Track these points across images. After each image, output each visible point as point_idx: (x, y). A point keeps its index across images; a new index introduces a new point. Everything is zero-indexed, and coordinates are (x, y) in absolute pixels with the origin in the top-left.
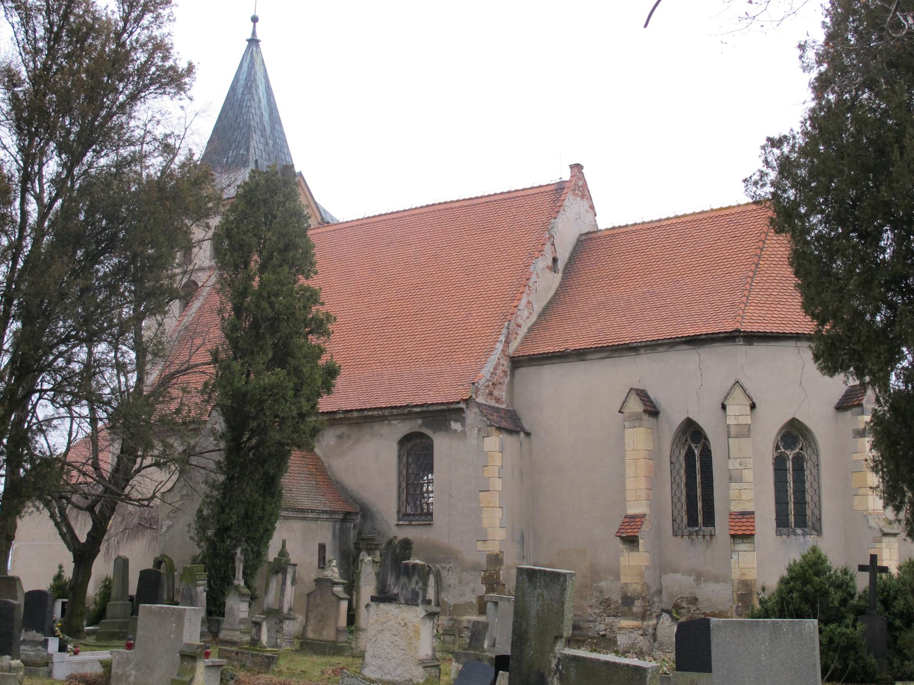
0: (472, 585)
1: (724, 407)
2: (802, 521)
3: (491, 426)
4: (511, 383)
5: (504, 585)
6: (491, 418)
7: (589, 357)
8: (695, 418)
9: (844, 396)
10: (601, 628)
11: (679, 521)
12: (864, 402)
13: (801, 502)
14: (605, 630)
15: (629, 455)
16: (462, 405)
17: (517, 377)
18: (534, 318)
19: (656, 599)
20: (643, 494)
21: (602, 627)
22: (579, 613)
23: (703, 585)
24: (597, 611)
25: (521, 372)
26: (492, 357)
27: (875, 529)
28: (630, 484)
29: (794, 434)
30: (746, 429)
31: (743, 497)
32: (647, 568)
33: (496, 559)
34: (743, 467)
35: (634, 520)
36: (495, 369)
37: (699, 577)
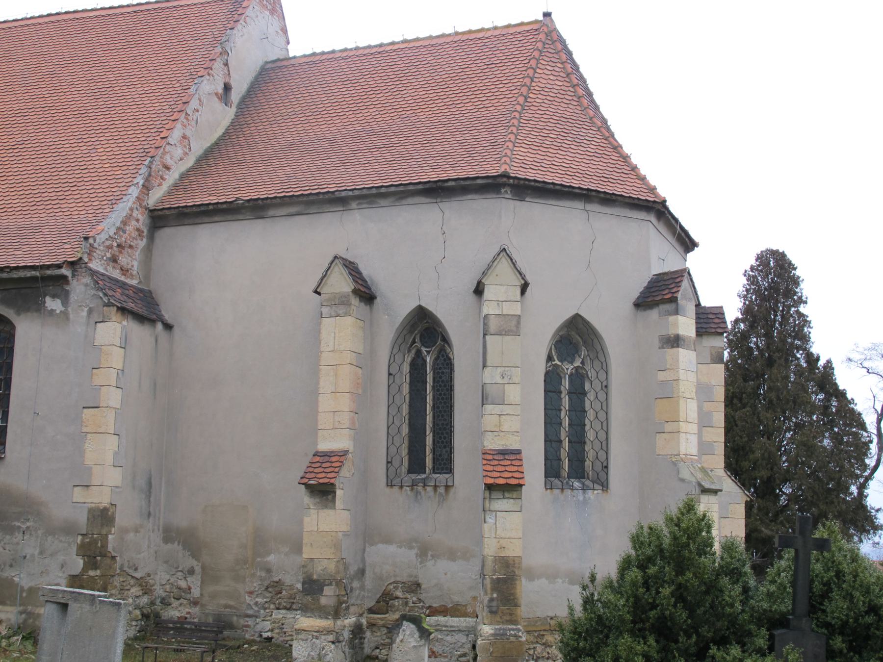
0: (61, 558)
1: (479, 291)
2: (578, 471)
3: (109, 305)
4: (149, 249)
5: (113, 558)
6: (110, 293)
7: (271, 212)
8: (430, 307)
9: (647, 288)
10: (265, 627)
11: (396, 463)
12: (679, 296)
13: (578, 440)
14: (272, 630)
15: (326, 358)
16: (65, 271)
17: (157, 241)
18: (190, 162)
19: (356, 584)
20: (345, 419)
21: (268, 625)
22: (232, 603)
23: (430, 563)
24: (259, 600)
25: (165, 234)
26: (121, 205)
27: (690, 482)
28: (325, 403)
29: (576, 338)
30: (514, 323)
31: (505, 428)
32: (346, 534)
33: (103, 517)
34: (506, 381)
35: (330, 460)
36: (124, 223)
37: (425, 551)
